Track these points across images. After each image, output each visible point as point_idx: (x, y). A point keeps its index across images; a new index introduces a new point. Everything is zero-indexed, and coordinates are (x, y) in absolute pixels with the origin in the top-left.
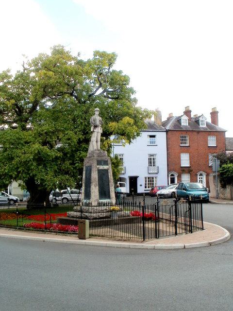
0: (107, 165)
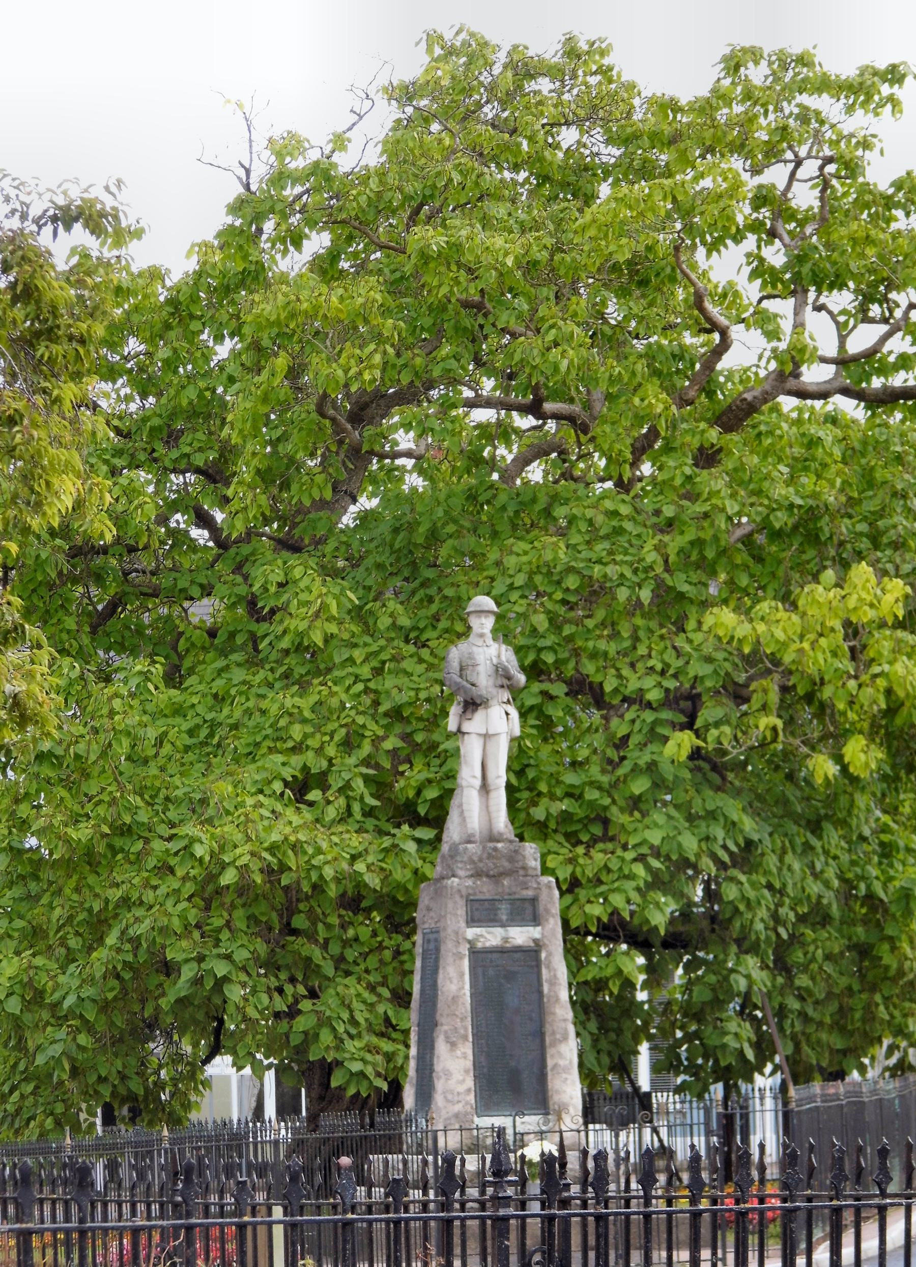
0: (536, 920)
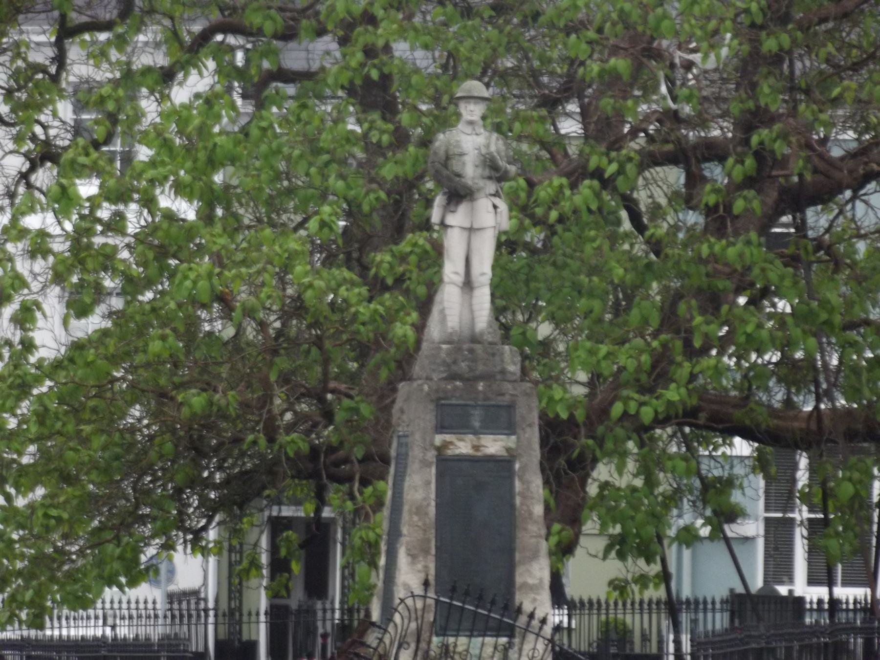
0: (510, 428)
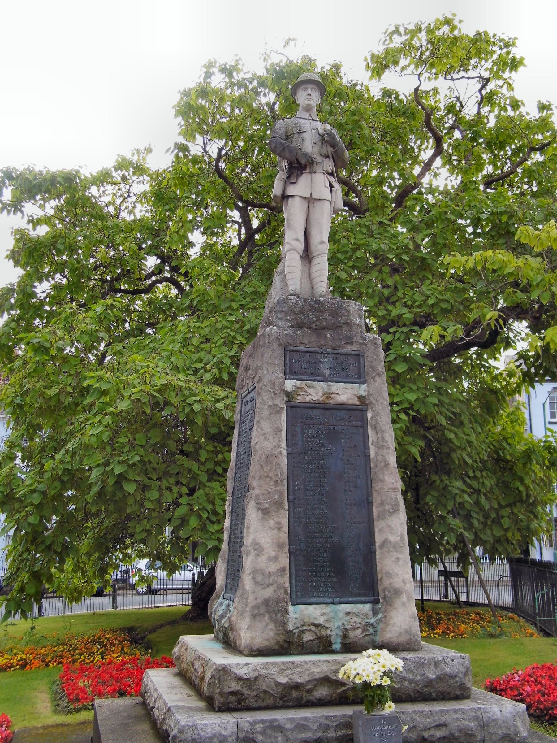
0: (360, 377)
